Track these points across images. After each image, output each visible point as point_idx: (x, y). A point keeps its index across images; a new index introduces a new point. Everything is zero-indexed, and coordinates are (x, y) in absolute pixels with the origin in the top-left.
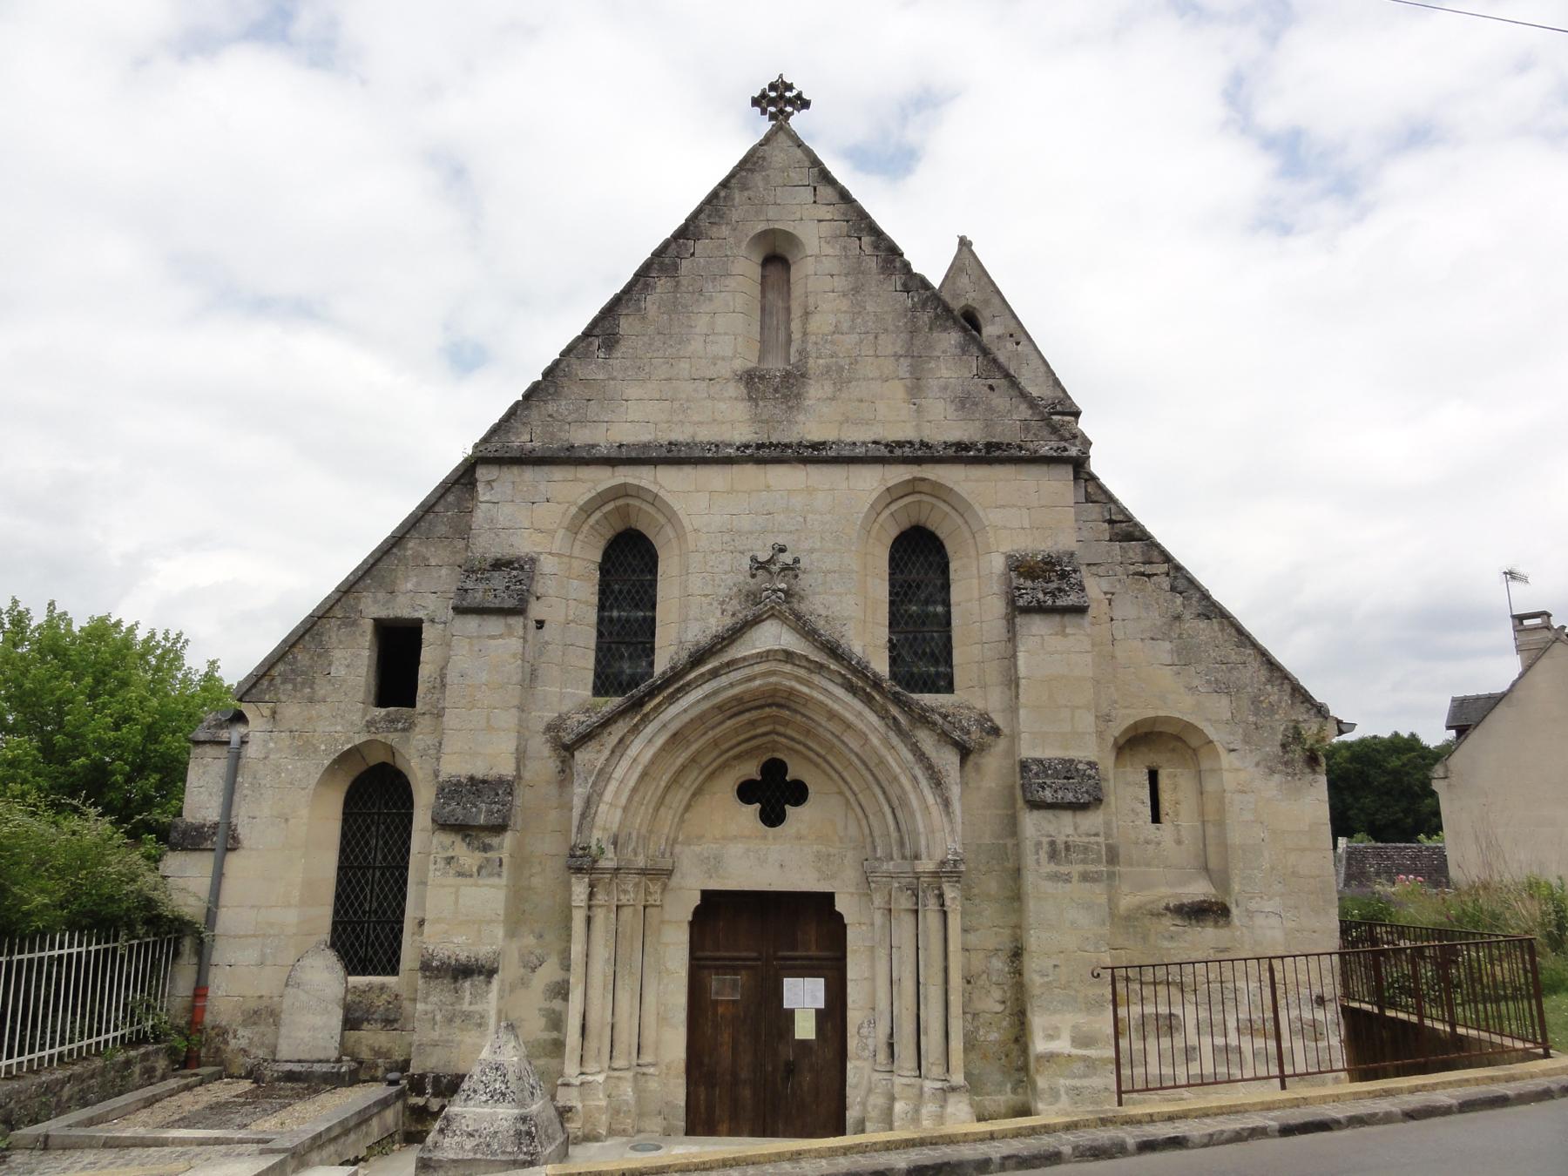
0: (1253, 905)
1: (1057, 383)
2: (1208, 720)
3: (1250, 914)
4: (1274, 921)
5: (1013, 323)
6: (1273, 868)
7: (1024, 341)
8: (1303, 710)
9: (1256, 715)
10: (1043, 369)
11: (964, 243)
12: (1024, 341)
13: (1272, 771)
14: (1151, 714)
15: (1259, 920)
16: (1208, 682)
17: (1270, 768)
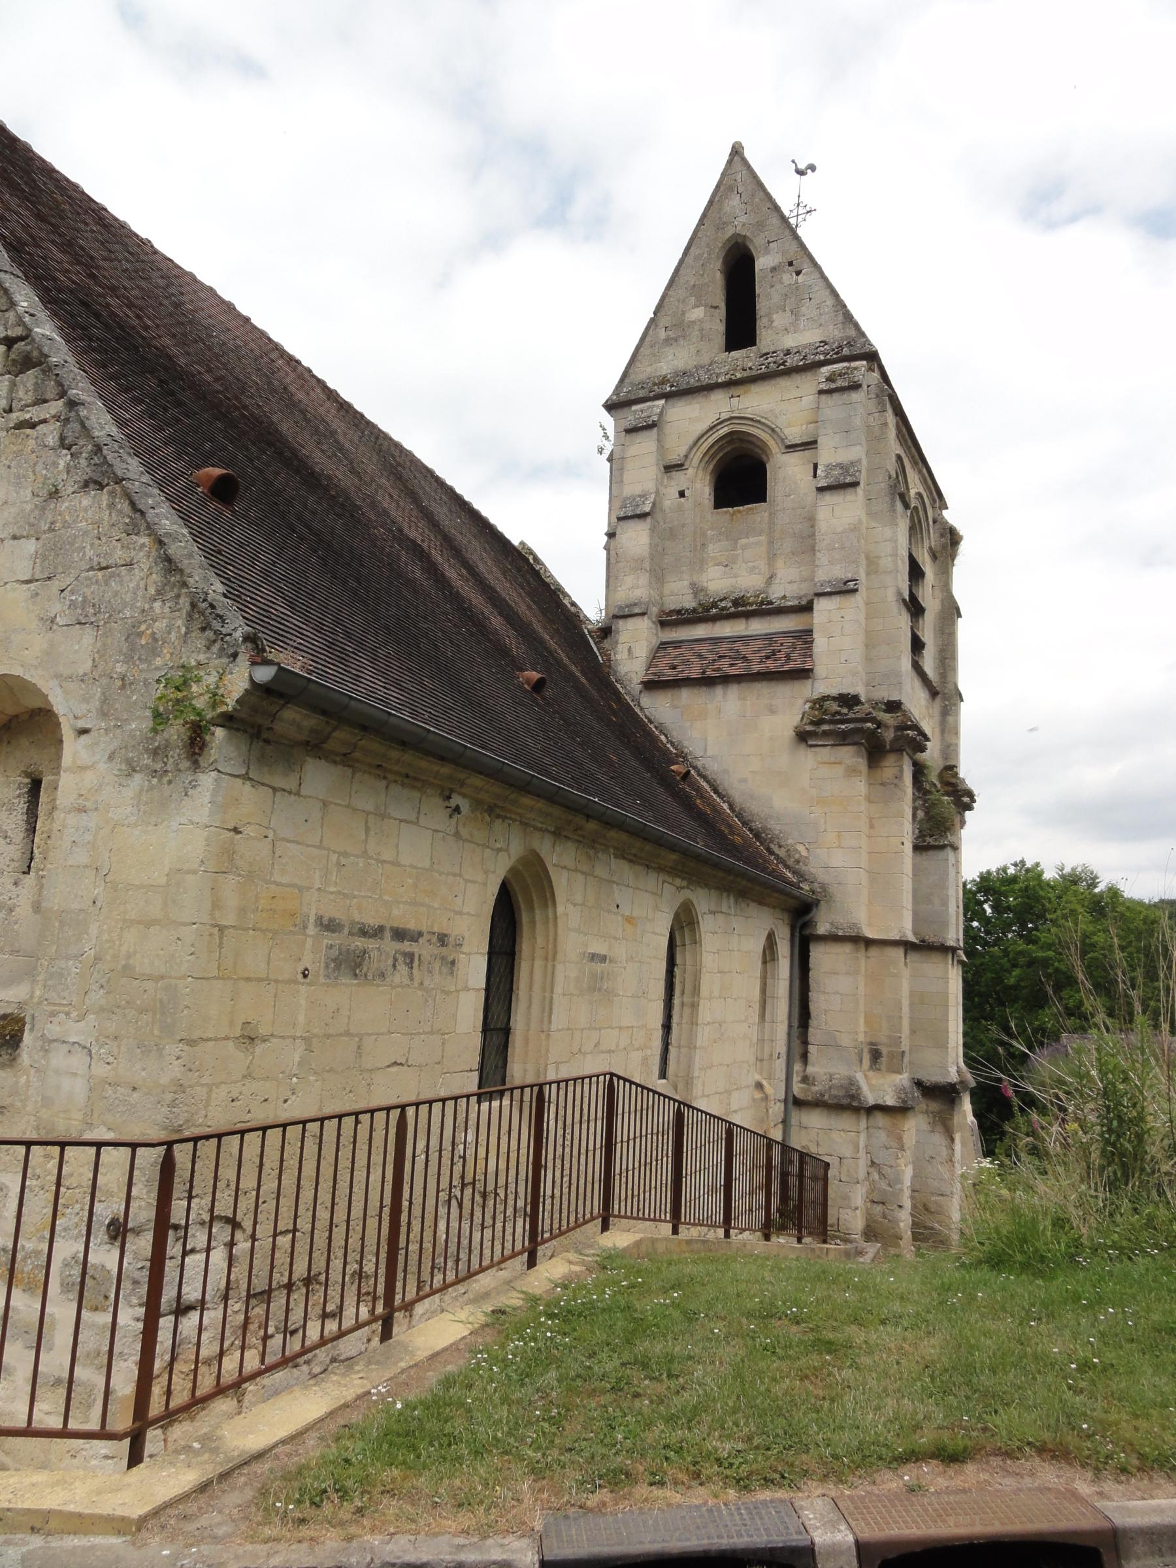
0: (53, 1029)
1: (848, 318)
2: (58, 676)
3: (47, 1044)
4: (78, 1061)
5: (794, 247)
6: (98, 959)
7: (807, 269)
8: (200, 644)
9: (128, 659)
10: (830, 302)
11: (737, 152)
12: (807, 269)
13: (132, 769)
14: (17, 671)
15: (58, 1059)
16: (73, 605)
17: (129, 762)
